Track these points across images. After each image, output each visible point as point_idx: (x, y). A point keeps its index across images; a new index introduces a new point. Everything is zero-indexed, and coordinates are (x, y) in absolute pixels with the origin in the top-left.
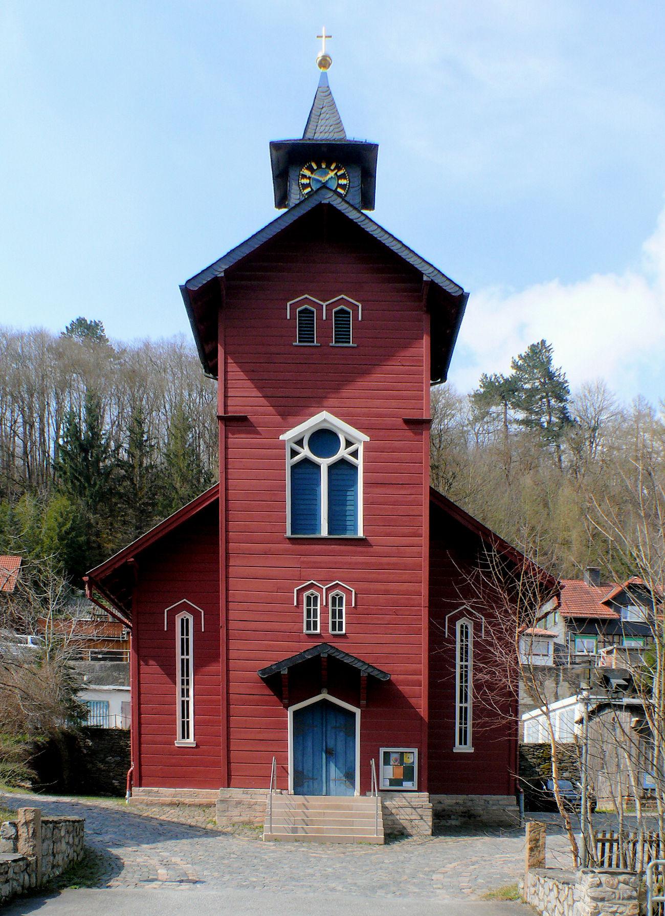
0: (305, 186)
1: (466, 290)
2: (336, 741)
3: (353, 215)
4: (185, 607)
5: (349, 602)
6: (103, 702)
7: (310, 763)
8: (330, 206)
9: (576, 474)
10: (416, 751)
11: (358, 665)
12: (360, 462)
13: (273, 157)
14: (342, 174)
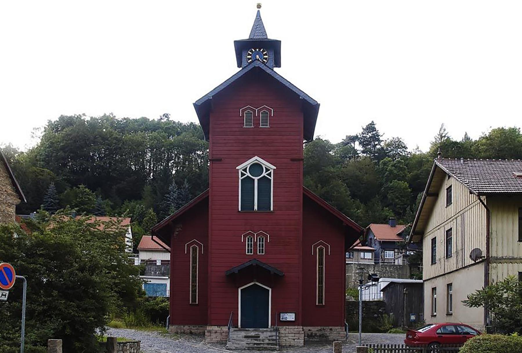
0: (249, 59)
1: (319, 103)
3: (269, 71)
4: (194, 243)
6: (164, 284)
8: (259, 67)
11: (269, 269)
12: (272, 178)
13: (236, 46)
14: (265, 54)
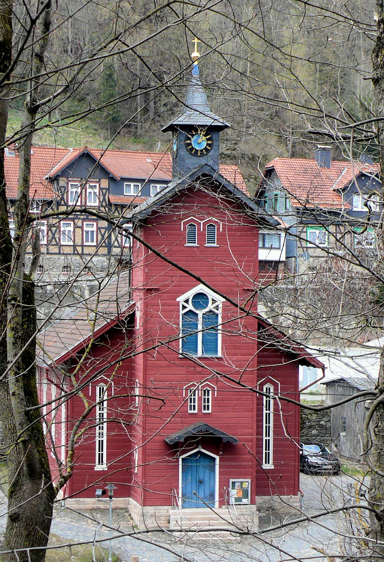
2: (203, 474)
5: (213, 394)
7: (190, 488)
9: (149, 16)
10: (249, 480)
12: (220, 312)
